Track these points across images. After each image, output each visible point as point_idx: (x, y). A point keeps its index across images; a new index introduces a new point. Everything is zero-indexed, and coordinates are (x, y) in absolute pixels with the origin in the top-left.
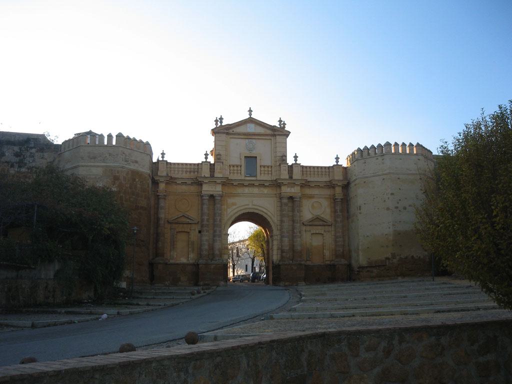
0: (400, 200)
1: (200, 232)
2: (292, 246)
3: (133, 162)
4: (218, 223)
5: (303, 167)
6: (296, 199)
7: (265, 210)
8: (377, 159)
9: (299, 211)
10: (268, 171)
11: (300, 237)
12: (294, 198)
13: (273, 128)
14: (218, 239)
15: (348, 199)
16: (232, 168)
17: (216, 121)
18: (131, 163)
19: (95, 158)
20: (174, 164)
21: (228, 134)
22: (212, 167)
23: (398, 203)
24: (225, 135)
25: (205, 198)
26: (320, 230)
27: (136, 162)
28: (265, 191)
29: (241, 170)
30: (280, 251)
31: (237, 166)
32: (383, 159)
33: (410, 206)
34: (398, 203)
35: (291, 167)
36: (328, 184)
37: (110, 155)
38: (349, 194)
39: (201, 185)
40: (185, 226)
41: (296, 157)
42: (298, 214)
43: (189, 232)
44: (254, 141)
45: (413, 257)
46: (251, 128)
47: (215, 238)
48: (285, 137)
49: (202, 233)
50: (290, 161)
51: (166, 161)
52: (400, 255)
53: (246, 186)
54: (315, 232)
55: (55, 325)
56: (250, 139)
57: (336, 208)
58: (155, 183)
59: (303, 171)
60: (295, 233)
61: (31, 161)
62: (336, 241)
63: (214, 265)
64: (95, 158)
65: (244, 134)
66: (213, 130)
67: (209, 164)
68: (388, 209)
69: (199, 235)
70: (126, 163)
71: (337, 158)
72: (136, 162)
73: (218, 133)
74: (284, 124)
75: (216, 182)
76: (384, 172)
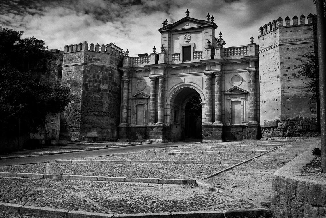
0: (289, 68)
8: (271, 34)
18: (94, 61)
68: (278, 77)
70: (89, 61)
71: (252, 38)
72: (99, 60)
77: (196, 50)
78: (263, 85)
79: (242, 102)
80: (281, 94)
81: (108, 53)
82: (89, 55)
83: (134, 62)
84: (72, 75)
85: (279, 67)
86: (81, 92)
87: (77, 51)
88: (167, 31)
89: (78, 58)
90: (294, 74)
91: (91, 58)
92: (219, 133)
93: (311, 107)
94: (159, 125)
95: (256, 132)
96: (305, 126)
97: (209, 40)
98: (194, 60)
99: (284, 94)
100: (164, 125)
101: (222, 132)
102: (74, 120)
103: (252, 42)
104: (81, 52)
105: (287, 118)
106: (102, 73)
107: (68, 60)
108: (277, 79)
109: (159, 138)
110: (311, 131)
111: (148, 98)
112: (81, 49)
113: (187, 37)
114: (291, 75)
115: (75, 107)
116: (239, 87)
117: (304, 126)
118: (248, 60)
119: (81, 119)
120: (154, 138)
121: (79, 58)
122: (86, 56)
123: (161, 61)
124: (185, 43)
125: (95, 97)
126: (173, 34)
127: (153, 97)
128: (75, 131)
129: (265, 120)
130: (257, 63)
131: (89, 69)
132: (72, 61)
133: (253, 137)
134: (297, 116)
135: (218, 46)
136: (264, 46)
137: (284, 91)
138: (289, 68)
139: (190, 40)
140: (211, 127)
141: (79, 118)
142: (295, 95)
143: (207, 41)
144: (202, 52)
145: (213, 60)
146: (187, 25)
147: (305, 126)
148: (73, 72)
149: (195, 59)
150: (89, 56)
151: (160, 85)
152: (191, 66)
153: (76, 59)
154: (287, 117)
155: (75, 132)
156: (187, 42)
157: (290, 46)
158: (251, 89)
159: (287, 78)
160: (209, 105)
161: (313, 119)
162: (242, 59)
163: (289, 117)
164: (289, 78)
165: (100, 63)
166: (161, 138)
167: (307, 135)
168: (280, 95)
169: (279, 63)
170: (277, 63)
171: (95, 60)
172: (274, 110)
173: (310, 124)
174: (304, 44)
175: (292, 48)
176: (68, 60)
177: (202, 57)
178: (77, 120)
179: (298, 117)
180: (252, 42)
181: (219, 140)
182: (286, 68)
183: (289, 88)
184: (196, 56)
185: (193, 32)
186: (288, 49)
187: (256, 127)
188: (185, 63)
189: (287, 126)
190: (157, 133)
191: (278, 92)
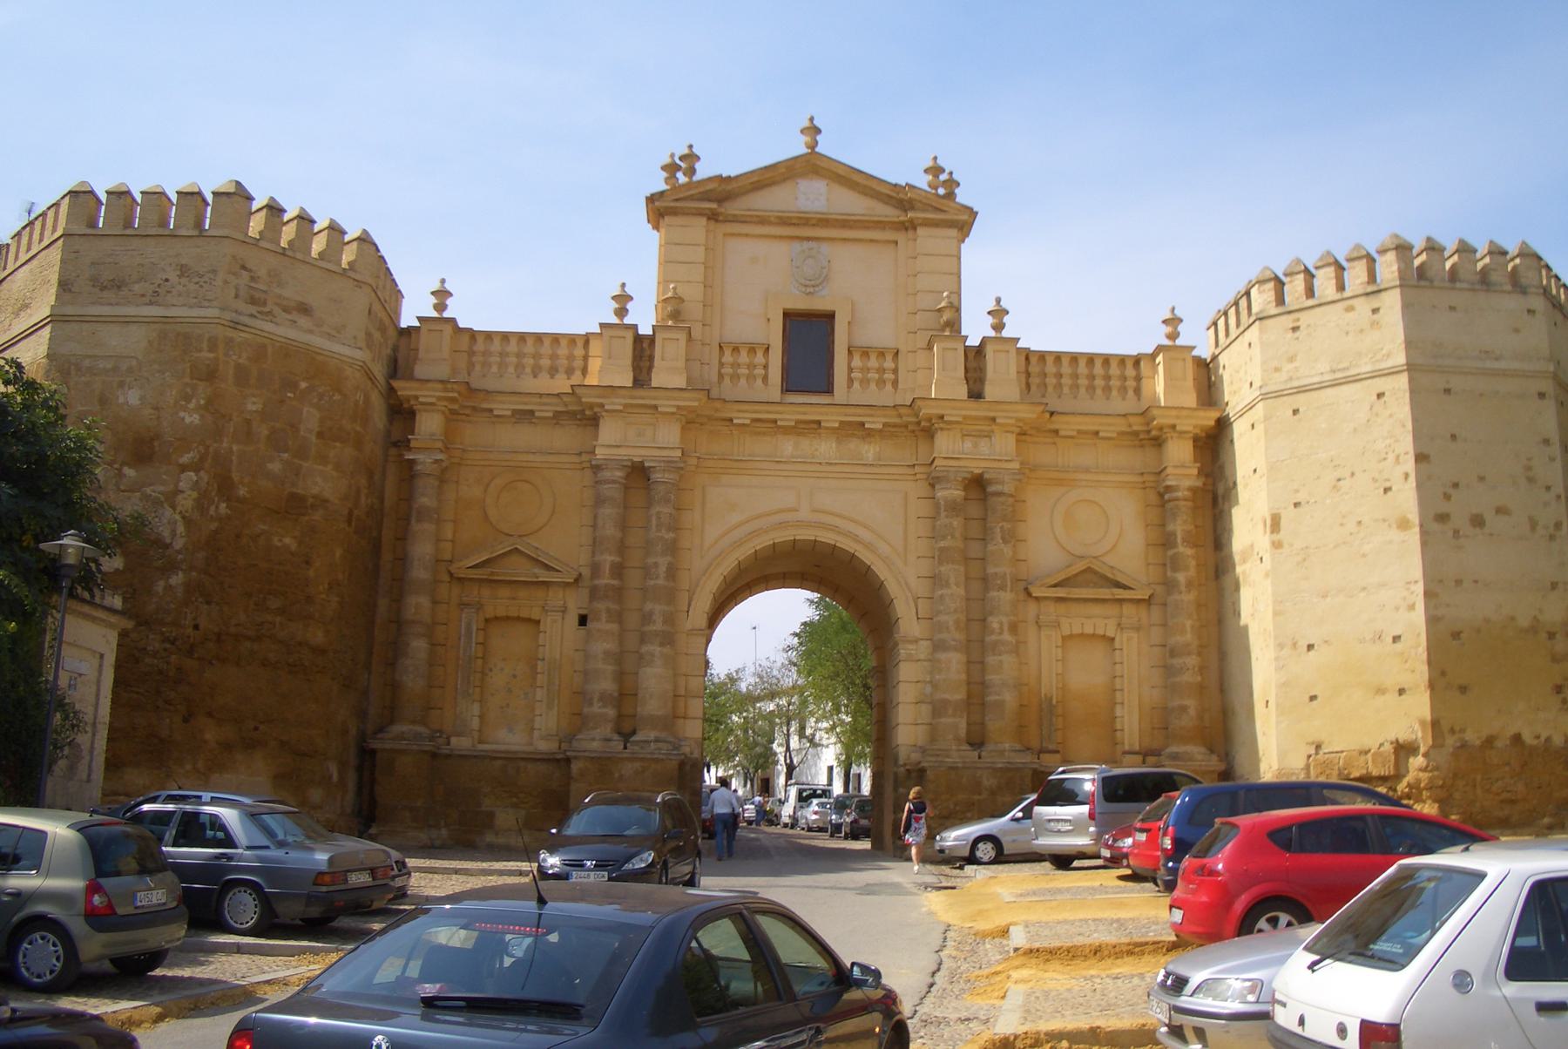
0: (1456, 485)
1: (583, 620)
2: (977, 697)
3: (286, 310)
4: (661, 582)
5: (1027, 354)
6: (998, 488)
7: (865, 535)
8: (1350, 309)
9: (1011, 537)
10: (882, 370)
11: (1017, 649)
12: (990, 482)
13: (900, 198)
14: (657, 649)
15: (1221, 491)
16: (728, 357)
17: (671, 169)
18: (277, 310)
19: (118, 285)
20: (489, 336)
21: (713, 217)
22: (643, 348)
24: (703, 221)
25: (607, 474)
26: (1100, 621)
27: (304, 309)
28: (869, 451)
29: (766, 367)
30: (925, 709)
31: (752, 350)
32: (1375, 311)
33: (1501, 511)
34: (1447, 497)
35: (976, 357)
36: (1135, 428)
37: (184, 271)
38: (1222, 468)
39: (594, 421)
40: (523, 593)
41: (999, 314)
42: (1007, 551)
43: (538, 622)
44: (825, 248)
45: (1517, 738)
46: (812, 196)
47: (644, 649)
48: (954, 232)
49: (590, 625)
50: (975, 328)
51: (453, 321)
52: (1463, 731)
53: (787, 431)
54: (1077, 630)
55: (729, 968)
56: (808, 239)
57: (1170, 527)
58: (402, 413)
59: (1028, 374)
60: (992, 632)
61: (791, 707)
62: (1168, 670)
63: (637, 765)
64: (118, 285)
65: (784, 221)
66: (651, 199)
67: (630, 336)
69: (582, 631)
70: (253, 309)
71: (1173, 321)
72: (304, 309)
73: (673, 212)
74: (952, 184)
75: (655, 407)
76: (1383, 365)
78: (1298, 564)
81: (358, 277)
82: (254, 268)
83: (478, 359)
84: (121, 385)
89: (173, 276)
91: (265, 292)
103: (1173, 336)
106: (321, 396)
108: (1395, 535)
111: (568, 584)
118: (591, 406)
121: (184, 280)
122: (234, 274)
123: (668, 373)
126: (725, 235)
129: (1311, 740)
131: (244, 355)
136: (1297, 364)
138: (1456, 485)
149: (856, 385)
150: (253, 279)
152: (515, 412)
154: (1457, 728)
159: (1451, 533)
160: (1121, 608)
162: (565, 399)
164: (1456, 533)
165: (311, 332)
170: (1391, 457)
171: (284, 311)
172: (1381, 691)
174: (1379, 376)
177: (895, 383)
180: (1173, 336)
184: (736, 365)
185: (845, 240)
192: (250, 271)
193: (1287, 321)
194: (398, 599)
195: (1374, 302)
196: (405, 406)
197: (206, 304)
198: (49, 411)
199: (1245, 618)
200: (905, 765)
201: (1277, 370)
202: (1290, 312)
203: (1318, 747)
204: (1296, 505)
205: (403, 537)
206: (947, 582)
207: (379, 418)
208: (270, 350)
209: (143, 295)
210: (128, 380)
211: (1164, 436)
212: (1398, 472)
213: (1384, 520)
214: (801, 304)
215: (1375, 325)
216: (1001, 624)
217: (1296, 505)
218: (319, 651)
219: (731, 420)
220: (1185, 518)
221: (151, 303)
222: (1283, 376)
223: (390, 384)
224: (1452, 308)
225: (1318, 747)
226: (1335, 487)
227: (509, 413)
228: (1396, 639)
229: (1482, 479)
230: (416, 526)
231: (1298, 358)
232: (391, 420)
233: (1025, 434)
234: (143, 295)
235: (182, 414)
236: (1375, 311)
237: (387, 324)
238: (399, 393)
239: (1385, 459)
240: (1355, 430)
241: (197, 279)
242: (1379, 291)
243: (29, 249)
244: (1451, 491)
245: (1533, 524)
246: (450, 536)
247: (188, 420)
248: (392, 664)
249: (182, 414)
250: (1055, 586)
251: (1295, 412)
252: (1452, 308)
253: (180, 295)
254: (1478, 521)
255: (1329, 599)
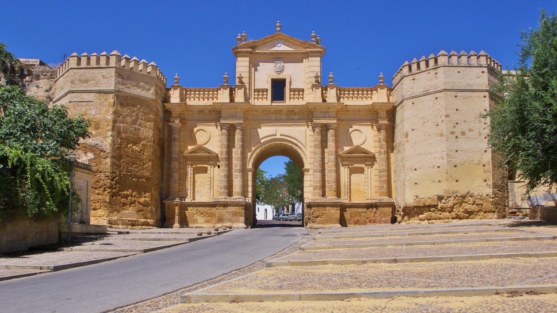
0: (457, 124)
8: (429, 73)
23: (454, 127)
33: (470, 130)
68: (441, 135)
77: (292, 87)
79: (366, 168)
80: (447, 158)
84: (90, 109)
85: (444, 121)
86: (109, 140)
87: (98, 66)
88: (247, 52)
89: (101, 78)
90: (463, 132)
92: (335, 213)
93: (486, 178)
94: (238, 200)
95: (391, 214)
96: (477, 205)
97: (317, 73)
98: (289, 101)
99: (450, 160)
100: (532, 205)
101: (340, 213)
102: (96, 189)
104: (108, 69)
105: (454, 194)
107: (80, 80)
108: (439, 138)
109: (238, 222)
110: (485, 212)
112: (108, 62)
113: (279, 64)
114: (460, 134)
115: (97, 165)
116: (362, 146)
117: (475, 204)
119: (109, 188)
120: (229, 220)
121: (104, 80)
124: (274, 73)
125: (132, 150)
127: (226, 155)
128: (98, 209)
130: (392, 113)
132: (89, 83)
133: (386, 220)
134: (467, 191)
135: (226, 84)
137: (450, 154)
138: (457, 124)
139: (282, 71)
140: (324, 205)
141: (105, 185)
142: (465, 162)
143: (315, 75)
144: (303, 90)
145: (324, 104)
146: (279, 45)
147: (477, 205)
148: (90, 103)
151: (238, 136)
153: (97, 80)
155: (99, 210)
156: (278, 72)
157: (458, 92)
158: (382, 151)
159: (455, 137)
160: (319, 172)
161: (487, 195)
163: (456, 192)
164: (457, 137)
166: (242, 222)
167: (480, 217)
168: (445, 161)
169: (444, 116)
170: (439, 116)
172: (434, 182)
173: (484, 202)
175: (461, 96)
176: (80, 80)
177: (303, 98)
178: (102, 189)
179: (468, 193)
181: (335, 224)
182: (454, 124)
183: (457, 151)
186: (456, 96)
187: (390, 207)
188: (273, 104)
189: (454, 205)
190: (235, 214)
191: (441, 156)
192: (122, 76)
193: (412, 77)
194: (169, 163)
195: (436, 71)
196: (168, 110)
197: (111, 86)
198: (9, 143)
199: (46, 253)
200: (306, 203)
201: (408, 91)
202: (412, 75)
203: (417, 197)
204: (413, 130)
205: (170, 146)
206: (317, 153)
207: (161, 114)
208: (129, 98)
209: (94, 84)
210: (91, 108)
211: (378, 111)
212: (440, 120)
213: (436, 134)
214: (276, 76)
215: (436, 78)
216: (331, 164)
217: (413, 130)
218: (148, 179)
219: (257, 111)
220: (384, 134)
221: (96, 86)
222: (410, 93)
223: (164, 105)
224: (459, 72)
225: (417, 197)
226: (423, 125)
227: (208, 111)
228: (439, 167)
229: (465, 121)
230: (173, 143)
231: (414, 88)
232: (165, 114)
233: (339, 111)
234: (94, 84)
235: (106, 116)
236: (436, 74)
237: (162, 88)
238: (166, 107)
239: (437, 116)
240: (429, 108)
241: (108, 79)
242: (437, 68)
243: (62, 72)
244: (456, 125)
245: (480, 134)
246: (183, 145)
247: (108, 118)
248: (168, 180)
249: (106, 116)
250: (189, 153)
251: (413, 103)
252: (459, 72)
253: (103, 84)
254: (463, 134)
255: (420, 156)
